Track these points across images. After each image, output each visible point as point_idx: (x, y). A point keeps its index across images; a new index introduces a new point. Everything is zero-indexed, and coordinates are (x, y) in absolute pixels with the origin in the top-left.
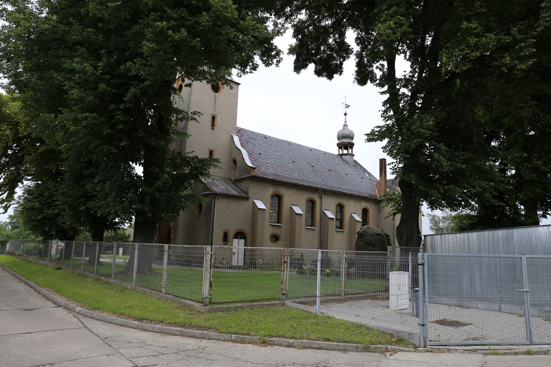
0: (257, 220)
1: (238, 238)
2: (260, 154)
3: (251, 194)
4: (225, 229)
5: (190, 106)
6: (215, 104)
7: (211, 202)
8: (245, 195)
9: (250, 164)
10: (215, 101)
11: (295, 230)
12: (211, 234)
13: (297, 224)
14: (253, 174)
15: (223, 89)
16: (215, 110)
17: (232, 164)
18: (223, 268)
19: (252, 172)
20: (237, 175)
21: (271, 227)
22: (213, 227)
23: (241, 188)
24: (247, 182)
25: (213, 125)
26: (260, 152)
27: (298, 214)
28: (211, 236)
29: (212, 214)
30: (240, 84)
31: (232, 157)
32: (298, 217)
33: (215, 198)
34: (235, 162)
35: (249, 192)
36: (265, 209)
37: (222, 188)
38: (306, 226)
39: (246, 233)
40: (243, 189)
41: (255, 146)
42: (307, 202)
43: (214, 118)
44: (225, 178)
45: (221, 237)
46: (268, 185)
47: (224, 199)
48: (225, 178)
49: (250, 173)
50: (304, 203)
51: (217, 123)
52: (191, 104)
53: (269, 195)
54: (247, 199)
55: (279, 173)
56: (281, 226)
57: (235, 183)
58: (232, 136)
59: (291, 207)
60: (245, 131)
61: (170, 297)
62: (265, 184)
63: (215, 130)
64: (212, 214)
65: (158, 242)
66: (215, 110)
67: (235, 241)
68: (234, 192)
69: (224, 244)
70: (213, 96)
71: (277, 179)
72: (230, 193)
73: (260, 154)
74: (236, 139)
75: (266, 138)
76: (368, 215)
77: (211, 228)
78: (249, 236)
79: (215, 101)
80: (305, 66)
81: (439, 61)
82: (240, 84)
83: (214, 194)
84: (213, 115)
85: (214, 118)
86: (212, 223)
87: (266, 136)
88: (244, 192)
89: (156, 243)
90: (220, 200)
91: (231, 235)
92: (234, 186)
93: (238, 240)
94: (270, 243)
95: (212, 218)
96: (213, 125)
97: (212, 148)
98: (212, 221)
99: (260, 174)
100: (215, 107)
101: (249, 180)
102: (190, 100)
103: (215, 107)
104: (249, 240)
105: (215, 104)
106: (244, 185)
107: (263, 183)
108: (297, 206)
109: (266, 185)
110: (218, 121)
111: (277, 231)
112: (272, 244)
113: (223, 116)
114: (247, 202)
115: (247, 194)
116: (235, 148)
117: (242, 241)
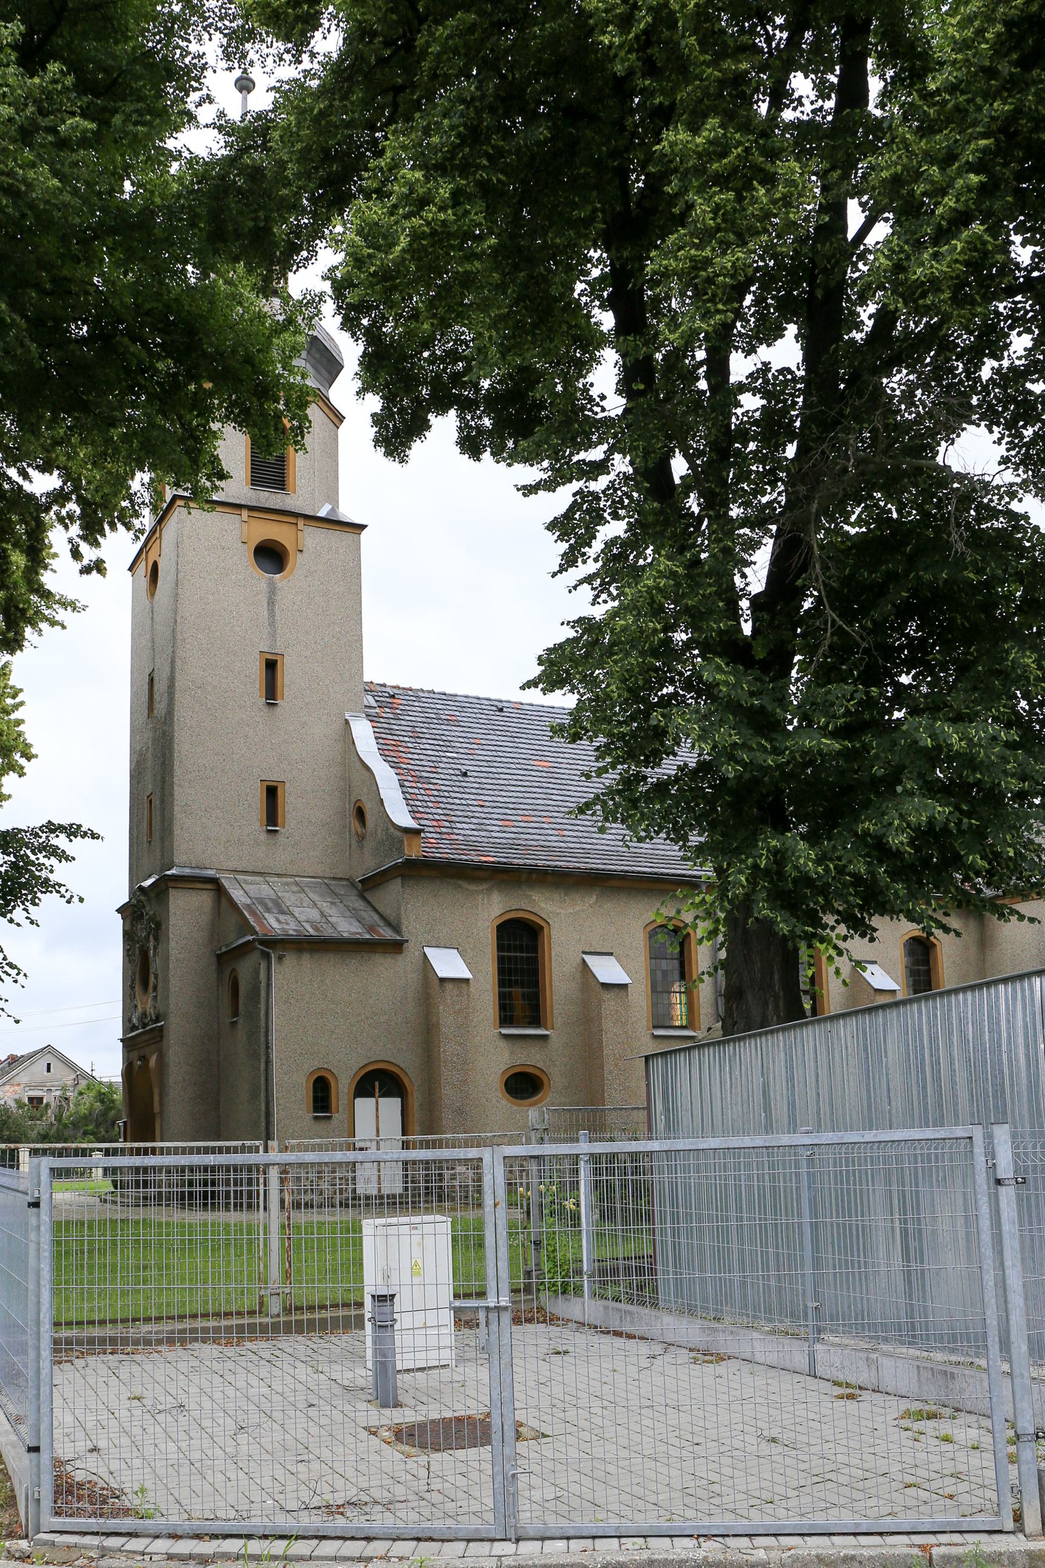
0: (438, 1024)
1: (372, 1095)
2: (465, 774)
3: (412, 927)
4: (317, 1064)
5: (179, 636)
6: (272, 613)
7: (257, 972)
8: (388, 934)
9: (402, 817)
10: (271, 603)
11: (601, 1049)
12: (263, 1087)
13: (607, 1024)
14: (414, 851)
15: (299, 555)
16: (273, 635)
17: (355, 824)
18: (320, 1206)
19: (409, 845)
20: (368, 864)
21: (503, 1044)
22: (268, 1062)
23: (381, 909)
24: (395, 886)
25: (271, 691)
26: (463, 768)
27: (606, 986)
28: (263, 1095)
29: (263, 1013)
30: (363, 527)
31: (353, 800)
32: (610, 1002)
33: (267, 957)
34: (360, 814)
35: (404, 921)
36: (467, 980)
37: (302, 918)
38: (655, 1027)
39: (402, 1075)
40: (387, 912)
41: (448, 745)
42: (652, 935)
43: (271, 665)
44: (334, 878)
45: (304, 1094)
46: (484, 886)
47: (306, 957)
48: (334, 878)
49: (400, 851)
50: (638, 942)
51: (286, 681)
52: (179, 628)
53: (487, 924)
54: (396, 947)
55: (534, 839)
56: (545, 1037)
57: (366, 895)
58: (347, 722)
59: (584, 961)
60: (415, 695)
61: (872, 1552)
62: (465, 885)
63: (278, 710)
64: (263, 1013)
65: (129, 1137)
66: (273, 635)
67: (364, 1106)
68: (347, 927)
69: (316, 1118)
70: (263, 586)
71: (516, 861)
72: (328, 932)
73: (465, 774)
74: (363, 733)
75: (501, 710)
76: (936, 963)
77: (263, 1066)
78: (413, 1081)
79: (271, 603)
80: (418, 427)
81: (215, 386)
82: (363, 527)
83: (263, 942)
84: (269, 657)
85: (271, 665)
86: (263, 1046)
87: (500, 705)
88: (389, 924)
89: (125, 1141)
90: (290, 960)
91: (343, 1086)
92: (359, 904)
93: (373, 1100)
94: (504, 1102)
95: (263, 1024)
96: (271, 691)
97: (274, 776)
98: (263, 1039)
99: (445, 852)
100: (272, 624)
101: (399, 880)
102: (176, 613)
103: (272, 624)
104: (416, 1098)
105: (272, 613)
106: (392, 895)
107: (460, 882)
108: (611, 954)
109: (473, 887)
110: (289, 675)
111: (530, 1058)
112: (515, 1108)
113: (308, 653)
114: (400, 958)
115: (396, 929)
116: (358, 764)
117: (391, 1106)
